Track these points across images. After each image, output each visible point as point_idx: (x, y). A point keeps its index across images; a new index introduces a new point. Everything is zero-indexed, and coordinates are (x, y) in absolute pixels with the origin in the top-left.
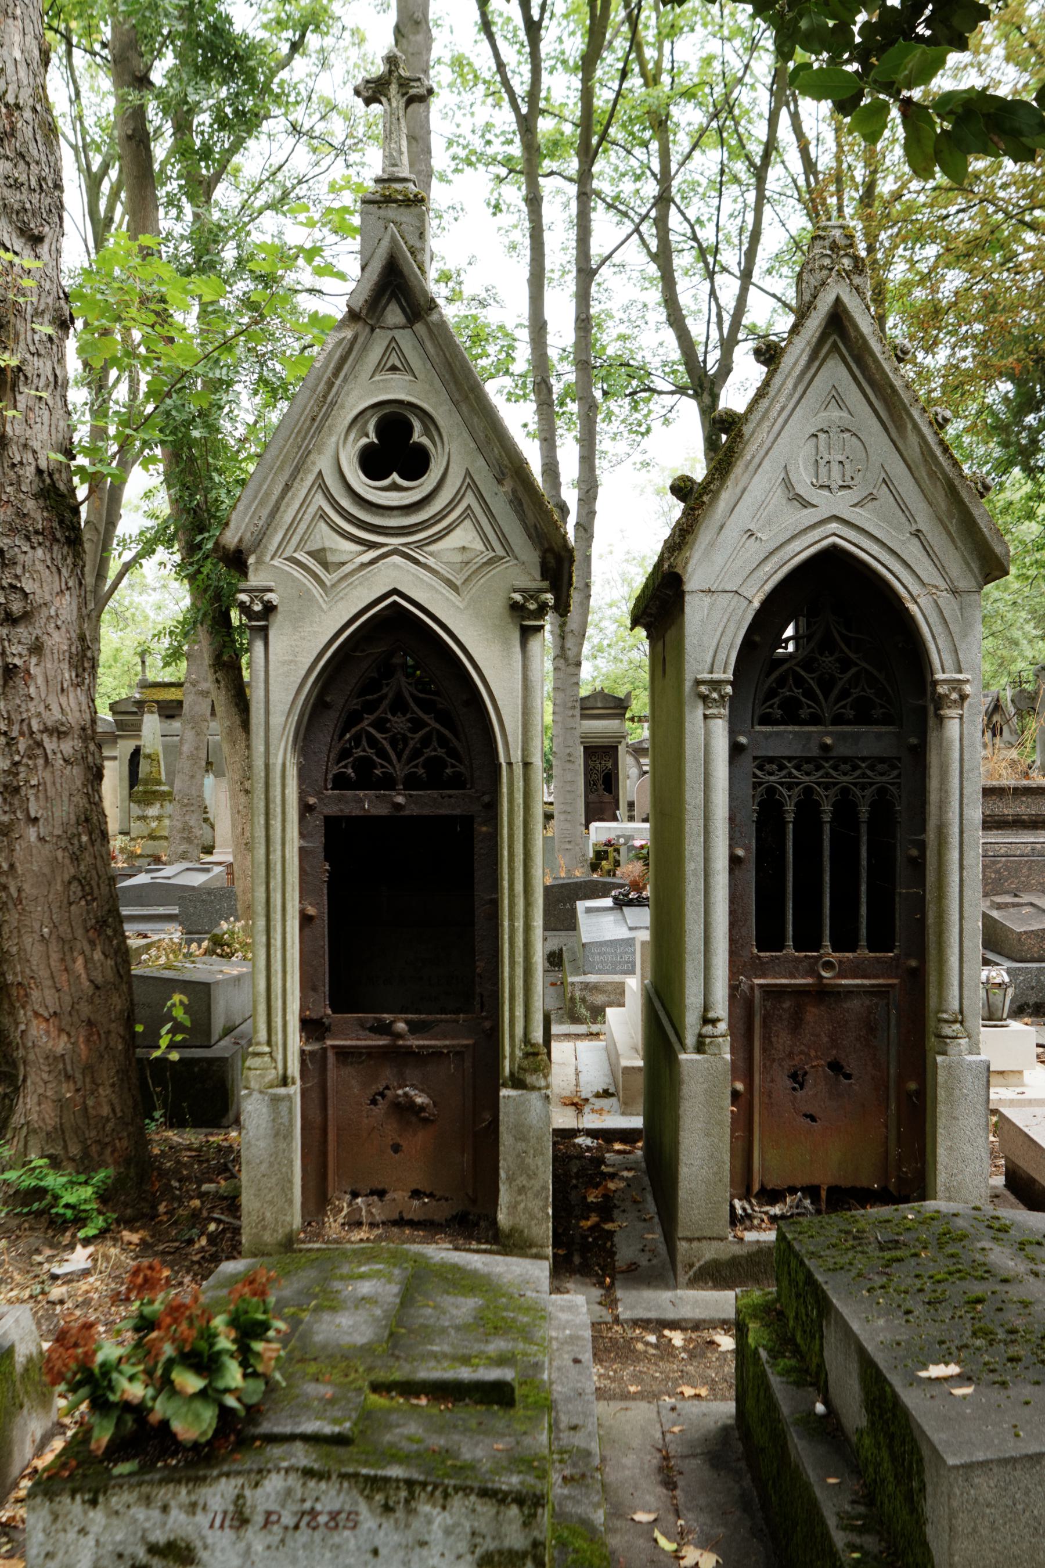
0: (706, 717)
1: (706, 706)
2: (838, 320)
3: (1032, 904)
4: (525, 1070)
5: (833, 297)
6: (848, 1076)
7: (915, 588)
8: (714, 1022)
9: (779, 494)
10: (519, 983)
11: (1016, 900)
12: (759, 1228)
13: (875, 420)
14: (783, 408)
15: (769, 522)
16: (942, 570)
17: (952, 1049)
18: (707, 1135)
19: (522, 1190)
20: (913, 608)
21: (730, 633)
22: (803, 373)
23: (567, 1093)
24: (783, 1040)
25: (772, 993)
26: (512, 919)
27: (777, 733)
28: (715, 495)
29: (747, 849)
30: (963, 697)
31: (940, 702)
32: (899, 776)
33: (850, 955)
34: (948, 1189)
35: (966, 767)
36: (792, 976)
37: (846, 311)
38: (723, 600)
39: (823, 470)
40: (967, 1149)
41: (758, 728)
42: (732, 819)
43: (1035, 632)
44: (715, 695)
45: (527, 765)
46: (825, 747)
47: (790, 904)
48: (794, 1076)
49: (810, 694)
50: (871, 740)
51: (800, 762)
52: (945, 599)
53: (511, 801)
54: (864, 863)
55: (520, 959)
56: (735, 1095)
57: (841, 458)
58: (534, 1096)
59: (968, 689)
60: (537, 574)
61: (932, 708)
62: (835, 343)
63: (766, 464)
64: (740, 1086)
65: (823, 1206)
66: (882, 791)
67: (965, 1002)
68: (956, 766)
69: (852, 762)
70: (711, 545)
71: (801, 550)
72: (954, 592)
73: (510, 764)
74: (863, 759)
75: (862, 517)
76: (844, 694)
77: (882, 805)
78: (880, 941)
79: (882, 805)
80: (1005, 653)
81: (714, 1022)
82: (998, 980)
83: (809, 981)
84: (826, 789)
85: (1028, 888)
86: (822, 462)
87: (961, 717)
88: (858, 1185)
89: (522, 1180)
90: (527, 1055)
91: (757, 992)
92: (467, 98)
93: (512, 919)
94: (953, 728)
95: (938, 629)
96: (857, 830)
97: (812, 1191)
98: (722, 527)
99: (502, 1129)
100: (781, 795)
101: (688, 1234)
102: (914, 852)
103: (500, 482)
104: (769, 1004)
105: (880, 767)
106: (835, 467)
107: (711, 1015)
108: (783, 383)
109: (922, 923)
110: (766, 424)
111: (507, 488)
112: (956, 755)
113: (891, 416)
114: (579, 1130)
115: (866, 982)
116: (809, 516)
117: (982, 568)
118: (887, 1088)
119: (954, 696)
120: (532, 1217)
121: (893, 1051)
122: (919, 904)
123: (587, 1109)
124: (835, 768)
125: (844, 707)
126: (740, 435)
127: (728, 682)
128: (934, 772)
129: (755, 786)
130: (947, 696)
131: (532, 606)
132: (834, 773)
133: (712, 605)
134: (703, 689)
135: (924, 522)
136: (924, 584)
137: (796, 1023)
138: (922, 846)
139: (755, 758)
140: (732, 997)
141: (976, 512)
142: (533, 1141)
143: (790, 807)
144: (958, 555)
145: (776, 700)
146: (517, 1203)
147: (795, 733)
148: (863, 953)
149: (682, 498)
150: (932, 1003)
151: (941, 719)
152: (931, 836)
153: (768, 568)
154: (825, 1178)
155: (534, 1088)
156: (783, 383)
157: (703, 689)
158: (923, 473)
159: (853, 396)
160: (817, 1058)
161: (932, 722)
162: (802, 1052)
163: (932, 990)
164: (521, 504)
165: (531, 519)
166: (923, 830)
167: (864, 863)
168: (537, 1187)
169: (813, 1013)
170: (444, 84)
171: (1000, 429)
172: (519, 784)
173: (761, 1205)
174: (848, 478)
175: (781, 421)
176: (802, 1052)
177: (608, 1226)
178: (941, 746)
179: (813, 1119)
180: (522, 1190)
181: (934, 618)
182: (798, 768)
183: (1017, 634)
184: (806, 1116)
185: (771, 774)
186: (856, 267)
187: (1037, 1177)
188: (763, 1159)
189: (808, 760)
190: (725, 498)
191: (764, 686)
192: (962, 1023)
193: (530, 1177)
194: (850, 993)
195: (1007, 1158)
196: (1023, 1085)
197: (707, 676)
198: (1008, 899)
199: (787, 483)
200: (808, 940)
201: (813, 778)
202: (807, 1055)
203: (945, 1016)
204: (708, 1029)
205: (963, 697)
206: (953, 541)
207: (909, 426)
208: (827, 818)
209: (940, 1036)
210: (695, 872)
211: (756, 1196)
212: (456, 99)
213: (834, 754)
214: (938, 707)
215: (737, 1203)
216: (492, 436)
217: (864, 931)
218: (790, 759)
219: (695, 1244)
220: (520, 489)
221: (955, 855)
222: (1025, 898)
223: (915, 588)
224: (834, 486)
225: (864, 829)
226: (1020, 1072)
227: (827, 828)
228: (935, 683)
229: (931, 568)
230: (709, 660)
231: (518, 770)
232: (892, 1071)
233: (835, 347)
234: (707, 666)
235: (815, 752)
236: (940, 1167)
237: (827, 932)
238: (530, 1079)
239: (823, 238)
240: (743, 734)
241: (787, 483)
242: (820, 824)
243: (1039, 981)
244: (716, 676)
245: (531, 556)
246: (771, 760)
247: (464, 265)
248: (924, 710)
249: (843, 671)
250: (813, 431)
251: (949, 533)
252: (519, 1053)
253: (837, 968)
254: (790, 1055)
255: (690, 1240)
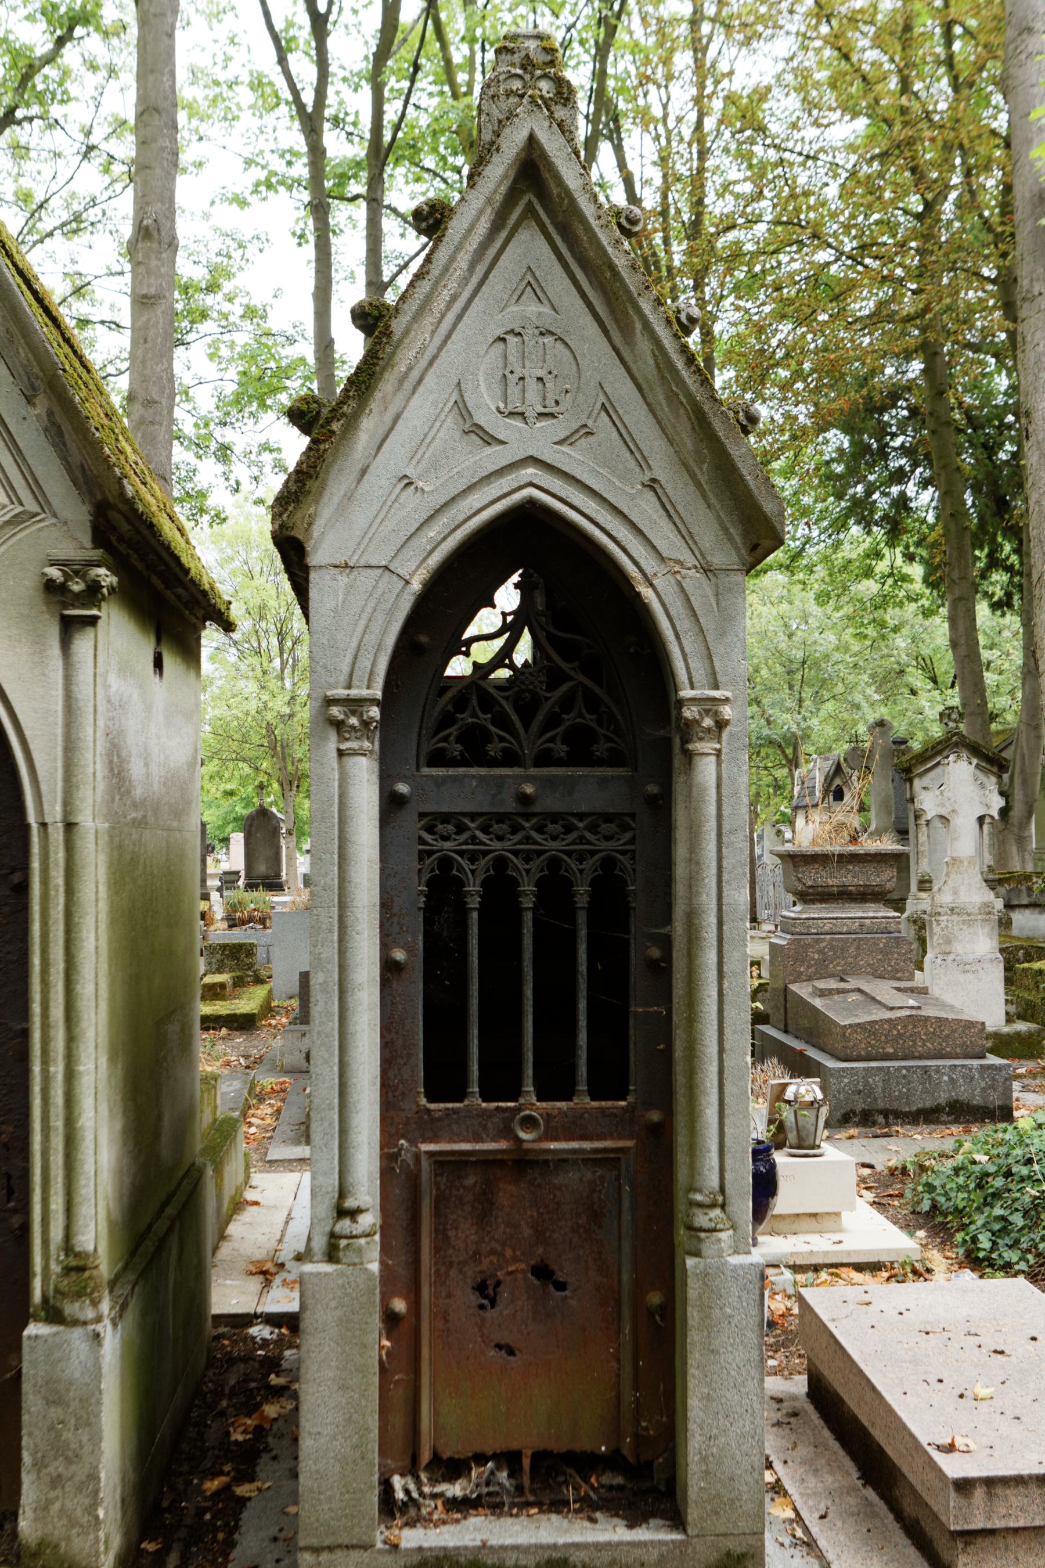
0: (341, 753)
1: (342, 739)
2: (533, 172)
3: (859, 990)
4: (64, 1295)
5: (525, 134)
6: (561, 1286)
7: (650, 564)
8: (353, 1214)
9: (451, 423)
10: (57, 1159)
11: (843, 985)
12: (427, 1521)
13: (589, 318)
14: (454, 298)
15: (435, 465)
16: (688, 538)
17: (708, 1248)
18: (343, 1387)
19: (56, 1482)
20: (647, 593)
21: (376, 628)
22: (484, 246)
23: (259, 1255)
24: (465, 1234)
25: (443, 1163)
26: (46, 1062)
27: (454, 779)
28: (352, 423)
29: (410, 950)
30: (721, 724)
31: (687, 730)
32: (632, 841)
33: (562, 1105)
34: (704, 1459)
35: (726, 827)
36: (478, 1139)
37: (544, 155)
38: (366, 579)
39: (514, 391)
40: (732, 1397)
41: (426, 771)
42: (386, 905)
43: (877, 697)
44: (354, 721)
45: (70, 827)
46: (525, 799)
47: (474, 1032)
48: (481, 1288)
49: (502, 721)
50: (592, 789)
51: (488, 821)
52: (693, 579)
53: (45, 882)
54: (583, 968)
55: (58, 1123)
56: (391, 1319)
57: (540, 373)
58: (76, 1334)
59: (727, 712)
60: (87, 540)
61: (677, 742)
62: (530, 203)
63: (430, 379)
64: (399, 1305)
65: (526, 1481)
66: (608, 863)
67: (728, 1176)
68: (711, 825)
69: (564, 821)
70: (349, 497)
71: (483, 507)
72: (707, 570)
73: (44, 825)
74: (581, 816)
75: (565, 458)
76: (553, 721)
77: (610, 886)
78: (608, 1082)
79: (610, 886)
80: (846, 716)
81: (353, 1214)
82: (809, 1098)
83: (503, 1145)
84: (527, 860)
85: (855, 971)
86: (513, 379)
87: (718, 754)
88: (577, 1447)
89: (57, 1466)
90: (68, 1270)
91: (425, 1164)
92: (270, 119)
93: (46, 1062)
94: (706, 770)
95: (684, 624)
96: (573, 921)
97: (510, 1459)
98: (364, 472)
99: (26, 1387)
100: (460, 869)
101: (314, 1541)
102: (655, 953)
103: (29, 400)
104: (443, 1181)
105: (605, 828)
106: (532, 385)
107: (350, 1203)
108: (452, 259)
109: (667, 1056)
110: (429, 320)
111: (41, 408)
112: (712, 809)
113: (612, 311)
114: (256, 1316)
115: (587, 1145)
116: (494, 457)
117: (745, 536)
118: (619, 1303)
119: (708, 722)
120: (73, 1523)
121: (626, 1246)
122: (663, 1029)
123: (277, 1281)
124: (540, 830)
125: (551, 740)
126: (388, 333)
127: (373, 701)
128: (681, 834)
129: (422, 856)
130: (698, 723)
131: (77, 586)
132: (588, 835)
133: (350, 588)
134: (335, 711)
135: (662, 468)
136: (662, 559)
137: (484, 1209)
138: (666, 943)
139: (422, 815)
140: (386, 1173)
141: (734, 452)
142: (74, 1405)
143: (528, 887)
144: (711, 515)
145: (453, 731)
146: (49, 1502)
147: (481, 779)
148: (583, 1102)
149: (306, 430)
150: (681, 1175)
151: (689, 756)
152: (678, 928)
153: (433, 532)
154: (527, 1441)
155: (75, 1323)
156: (452, 259)
157: (335, 711)
158: (659, 396)
159: (557, 283)
160: (515, 1259)
161: (678, 761)
162: (493, 1252)
163: (681, 1157)
164: (60, 434)
165: (76, 457)
166: (668, 919)
167: (583, 968)
168: (81, 1476)
169: (507, 1193)
170: (244, 106)
171: (837, 485)
172: (58, 855)
173: (434, 1481)
174: (550, 402)
175: (451, 317)
176: (493, 1252)
177: (242, 1490)
178: (689, 796)
179: (511, 1352)
180: (56, 1482)
181: (677, 608)
182: (485, 830)
183: (858, 698)
184: (499, 1347)
185: (445, 839)
186: (559, 93)
187: (845, 1397)
188: (436, 1413)
189: (501, 818)
190: (368, 427)
191: (420, 707)
192: (723, 1207)
193: (69, 1461)
194: (562, 1161)
195: (809, 1360)
196: (840, 1230)
197: (341, 692)
198: (833, 984)
199: (462, 409)
200: (501, 1083)
201: (507, 844)
202: (501, 1255)
203: (699, 1197)
204: (345, 1225)
205: (721, 724)
206: (704, 496)
207: (638, 326)
208: (528, 902)
209: (690, 1228)
210: (325, 987)
211: (428, 1467)
212: (257, 122)
213: (537, 808)
214: (686, 740)
215: (397, 1482)
216: (14, 329)
217: (583, 1070)
218: (473, 816)
219: (324, 1557)
220: (57, 410)
221: (710, 957)
222: (853, 983)
223: (650, 564)
224: (530, 414)
225: (582, 918)
226: (838, 1214)
227: (528, 917)
228: (680, 703)
229: (673, 535)
230: (346, 669)
231: (57, 835)
232: (625, 1277)
233: (530, 211)
234: (343, 678)
235: (510, 806)
236: (692, 1426)
237: (529, 1071)
238: (71, 1309)
239: (511, 51)
240: (403, 779)
241: (462, 409)
242: (519, 911)
243: (866, 1083)
244: (354, 693)
245: (78, 514)
246: (445, 818)
247: (270, 300)
248: (668, 742)
249: (551, 688)
250: (499, 332)
251: (698, 485)
252: (55, 1268)
253: (541, 1124)
254: (476, 1256)
255: (317, 1550)
